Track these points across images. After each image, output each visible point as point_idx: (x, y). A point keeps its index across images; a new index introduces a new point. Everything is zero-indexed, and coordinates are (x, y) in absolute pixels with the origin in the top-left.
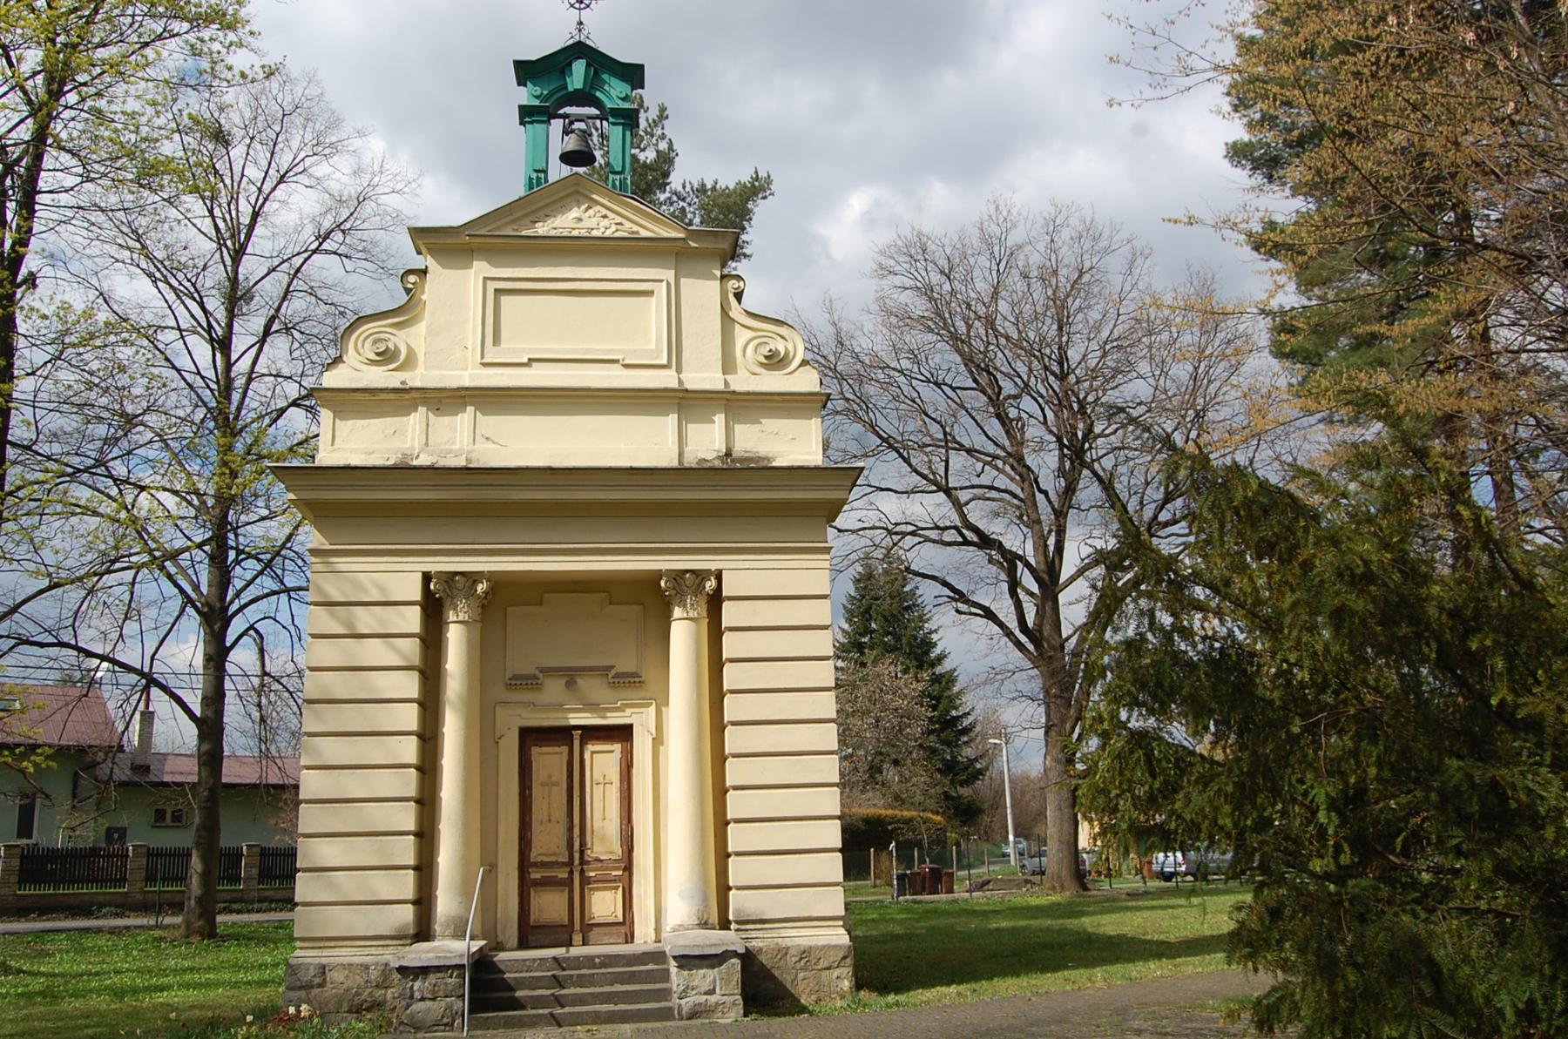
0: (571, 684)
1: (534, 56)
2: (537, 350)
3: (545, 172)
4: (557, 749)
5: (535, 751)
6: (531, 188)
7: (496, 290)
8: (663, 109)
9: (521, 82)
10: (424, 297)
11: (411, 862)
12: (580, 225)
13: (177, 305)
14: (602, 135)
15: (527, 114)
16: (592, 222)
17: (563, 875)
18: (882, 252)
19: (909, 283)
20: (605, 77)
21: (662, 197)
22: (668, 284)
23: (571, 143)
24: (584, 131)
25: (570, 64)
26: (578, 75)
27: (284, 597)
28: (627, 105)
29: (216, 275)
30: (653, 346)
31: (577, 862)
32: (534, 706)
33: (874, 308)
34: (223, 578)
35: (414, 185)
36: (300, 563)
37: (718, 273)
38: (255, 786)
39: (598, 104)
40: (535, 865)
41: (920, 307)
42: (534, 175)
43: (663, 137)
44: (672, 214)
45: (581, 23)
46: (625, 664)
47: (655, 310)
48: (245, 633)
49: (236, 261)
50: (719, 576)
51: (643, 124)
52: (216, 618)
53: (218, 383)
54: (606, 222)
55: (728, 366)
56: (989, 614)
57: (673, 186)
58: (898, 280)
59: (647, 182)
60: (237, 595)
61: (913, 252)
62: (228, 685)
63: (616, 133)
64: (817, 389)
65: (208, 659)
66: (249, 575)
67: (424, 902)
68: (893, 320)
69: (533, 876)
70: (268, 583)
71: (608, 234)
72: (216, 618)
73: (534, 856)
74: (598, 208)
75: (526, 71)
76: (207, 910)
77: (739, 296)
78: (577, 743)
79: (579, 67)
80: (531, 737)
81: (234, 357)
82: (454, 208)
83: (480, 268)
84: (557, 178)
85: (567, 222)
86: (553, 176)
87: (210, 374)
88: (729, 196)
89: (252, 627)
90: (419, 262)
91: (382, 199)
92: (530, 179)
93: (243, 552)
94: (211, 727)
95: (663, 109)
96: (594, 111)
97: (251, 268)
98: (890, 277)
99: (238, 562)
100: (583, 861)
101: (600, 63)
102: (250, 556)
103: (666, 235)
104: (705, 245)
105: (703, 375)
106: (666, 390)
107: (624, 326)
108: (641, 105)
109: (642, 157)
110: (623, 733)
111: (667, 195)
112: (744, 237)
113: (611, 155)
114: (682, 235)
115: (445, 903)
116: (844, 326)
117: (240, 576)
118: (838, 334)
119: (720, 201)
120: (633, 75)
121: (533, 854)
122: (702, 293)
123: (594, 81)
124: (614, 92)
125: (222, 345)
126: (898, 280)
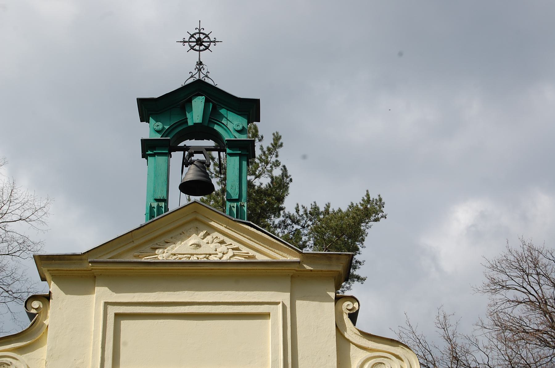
3: (165, 201)
6: (152, 216)
7: (117, 315)
8: (277, 138)
9: (144, 118)
10: (46, 322)
12: (199, 251)
14: (220, 165)
15: (149, 148)
16: (210, 249)
18: (493, 267)
19: (522, 296)
20: (223, 111)
21: (277, 221)
22: (284, 307)
23: (191, 173)
24: (202, 162)
25: (190, 101)
28: (243, 137)
33: (488, 322)
35: (40, 213)
37: (332, 295)
39: (216, 136)
41: (535, 320)
42: (155, 204)
43: (277, 164)
44: (286, 238)
45: (200, 63)
47: (271, 331)
51: (258, 152)
54: (223, 248)
57: (286, 211)
58: (511, 294)
59: (262, 207)
61: (525, 266)
63: (233, 164)
68: (508, 334)
71: (225, 258)
74: (216, 234)
75: (148, 108)
77: (353, 317)
79: (198, 104)
82: (80, 236)
83: (102, 294)
84: (176, 207)
85: (188, 247)
86: (173, 205)
88: (342, 218)
90: (42, 288)
91: (10, 226)
92: (151, 208)
95: (277, 138)
96: (211, 143)
98: (503, 292)
101: (218, 100)
103: (281, 258)
104: (319, 268)
108: (255, 135)
109: (257, 183)
111: (281, 218)
112: (357, 257)
113: (229, 182)
114: (296, 259)
116: (459, 341)
118: (453, 349)
119: (333, 224)
120: (250, 109)
122: (317, 316)
123: (212, 115)
124: (232, 125)
126: (511, 294)
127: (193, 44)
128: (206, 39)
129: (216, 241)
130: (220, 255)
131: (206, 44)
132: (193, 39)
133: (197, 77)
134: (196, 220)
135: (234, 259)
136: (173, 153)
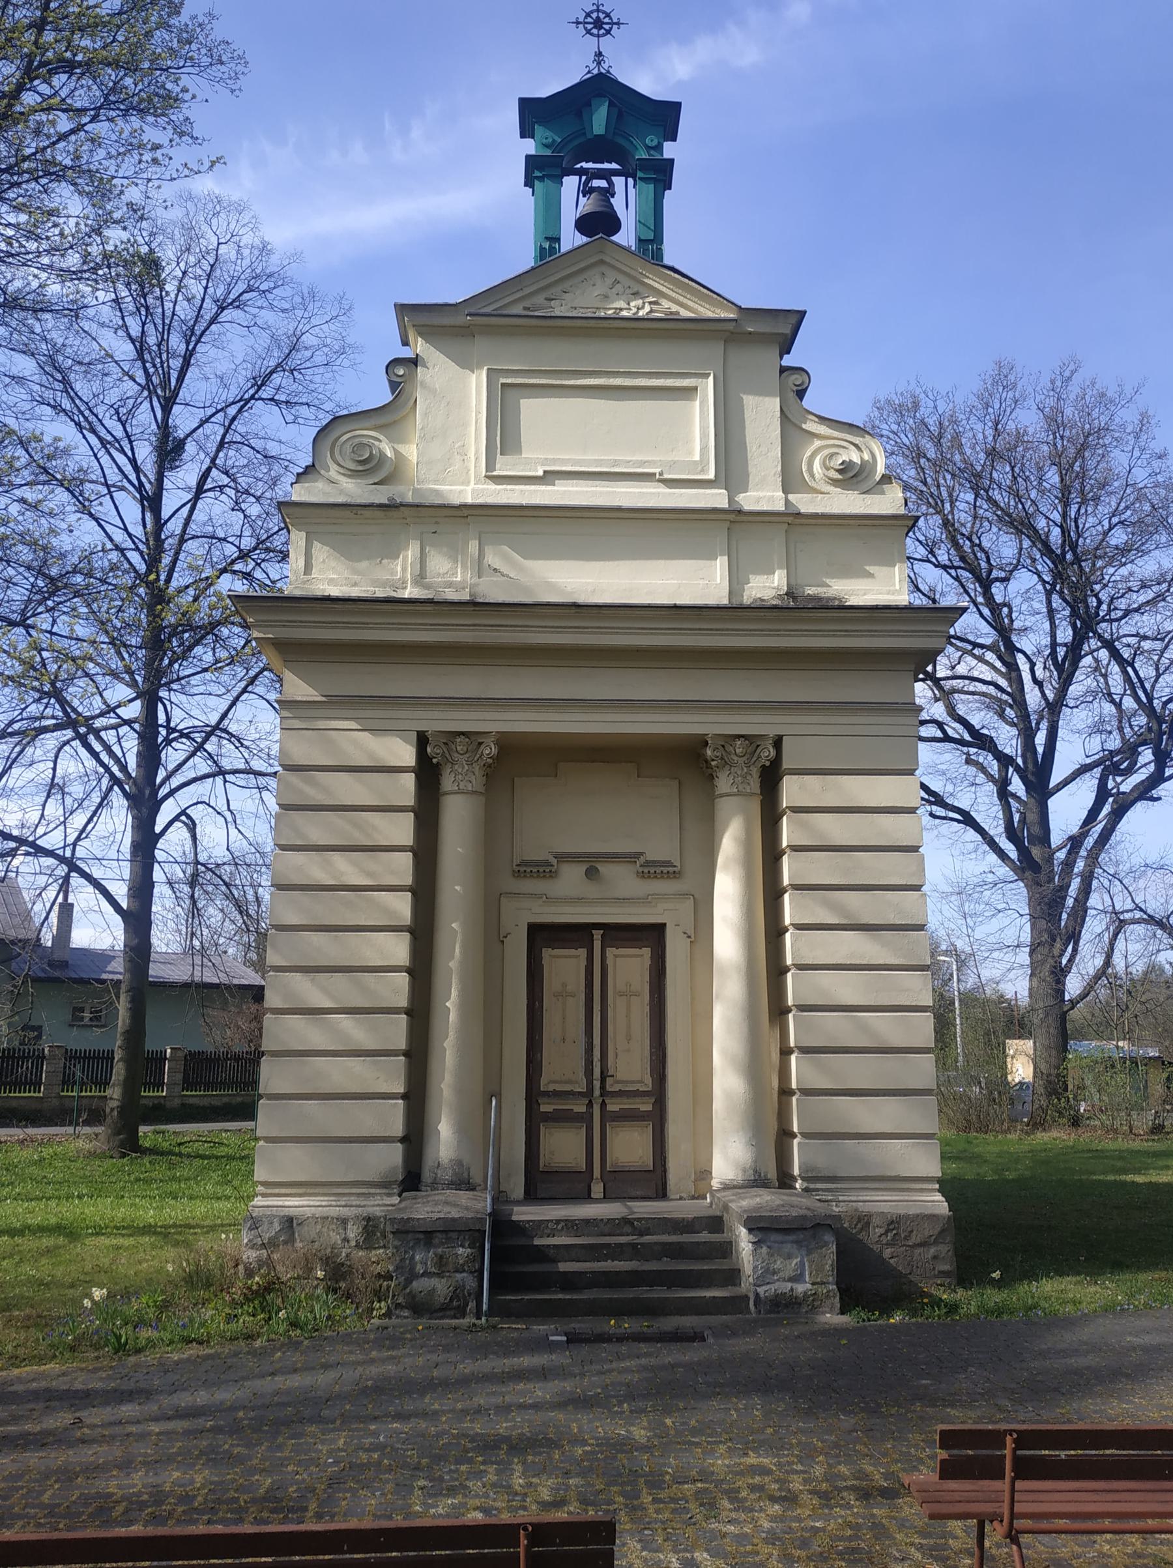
0: (592, 873)
1: (544, 92)
2: (554, 461)
3: (558, 240)
4: (572, 952)
5: (547, 953)
11: (400, 1089)
13: (105, 460)
17: (581, 1108)
23: (587, 205)
25: (589, 104)
26: (599, 121)
27: (219, 780)
29: (145, 418)
30: (697, 458)
31: (597, 1092)
32: (549, 900)
34: (150, 755)
36: (238, 745)
38: (186, 986)
40: (547, 1094)
42: (547, 245)
45: (599, 54)
46: (660, 848)
47: (698, 417)
48: (176, 818)
49: (167, 410)
50: (778, 742)
52: (144, 800)
53: (147, 544)
55: (791, 481)
56: (968, 819)
60: (168, 777)
62: (158, 875)
64: (902, 511)
65: (136, 847)
66: (181, 756)
67: (415, 1137)
69: (544, 1108)
70: (201, 765)
71: (641, 313)
72: (144, 800)
73: (545, 1084)
75: (533, 113)
76: (133, 1116)
78: (597, 945)
80: (543, 936)
81: (165, 514)
84: (570, 247)
86: (566, 245)
87: (138, 531)
89: (183, 812)
92: (542, 249)
93: (174, 730)
94: (138, 919)
97: (183, 420)
99: (168, 742)
100: (604, 1092)
102: (183, 735)
103: (710, 315)
105: (765, 494)
106: (715, 510)
107: (651, 440)
110: (652, 936)
115: (445, 1138)
117: (172, 756)
121: (544, 1081)
125: (152, 502)
127: (589, 26)
128: (607, 20)
129: (628, 291)
130: (634, 310)
131: (607, 27)
132: (589, 20)
133: (595, 72)
134: (602, 262)
135: (650, 316)
136: (565, 179)
